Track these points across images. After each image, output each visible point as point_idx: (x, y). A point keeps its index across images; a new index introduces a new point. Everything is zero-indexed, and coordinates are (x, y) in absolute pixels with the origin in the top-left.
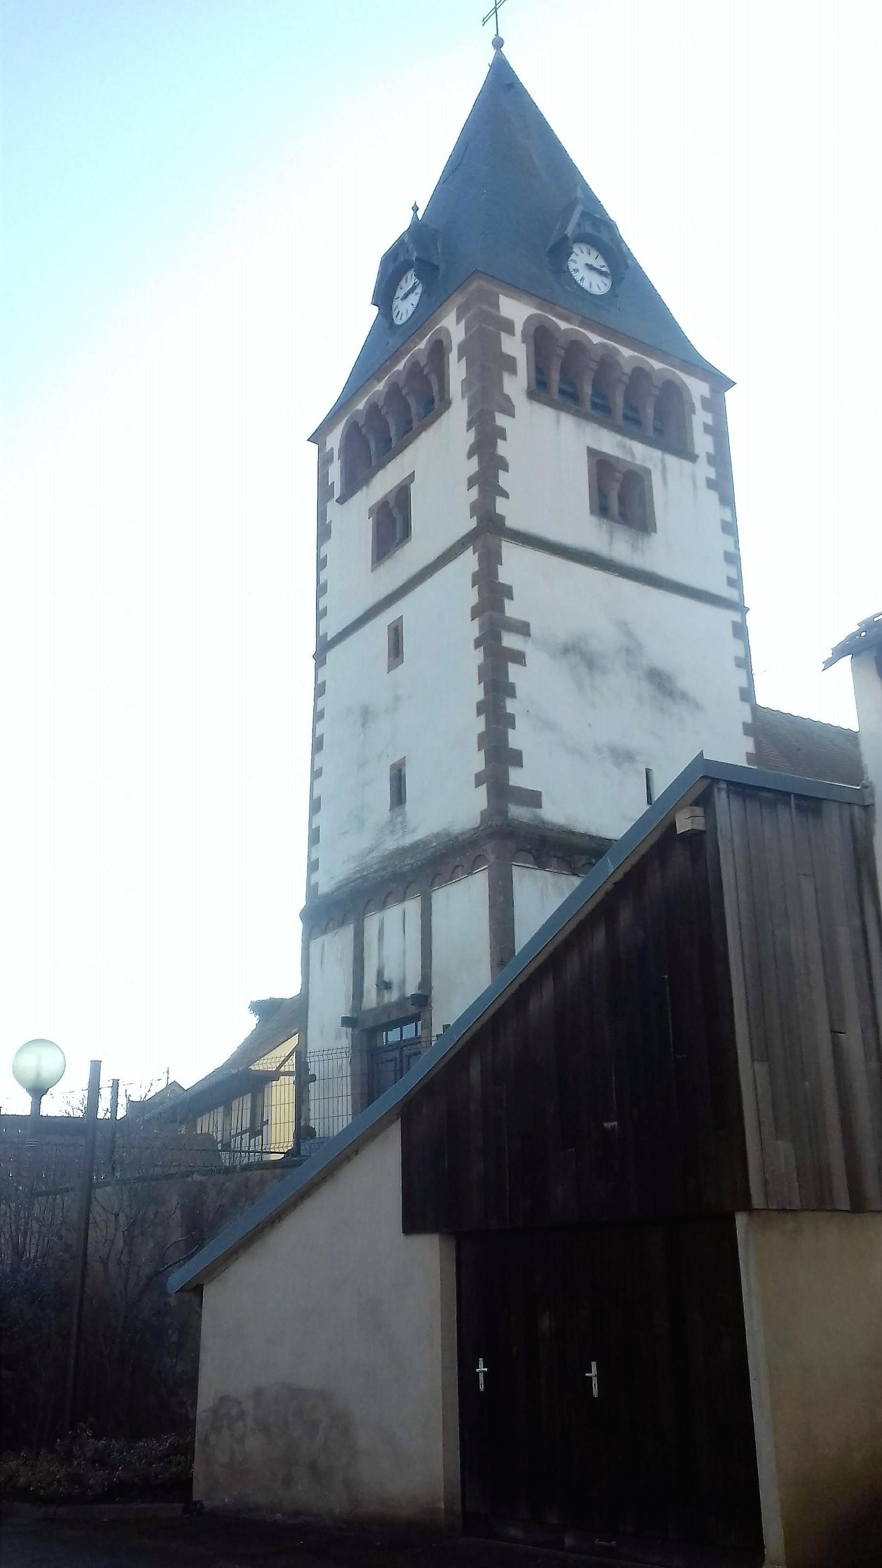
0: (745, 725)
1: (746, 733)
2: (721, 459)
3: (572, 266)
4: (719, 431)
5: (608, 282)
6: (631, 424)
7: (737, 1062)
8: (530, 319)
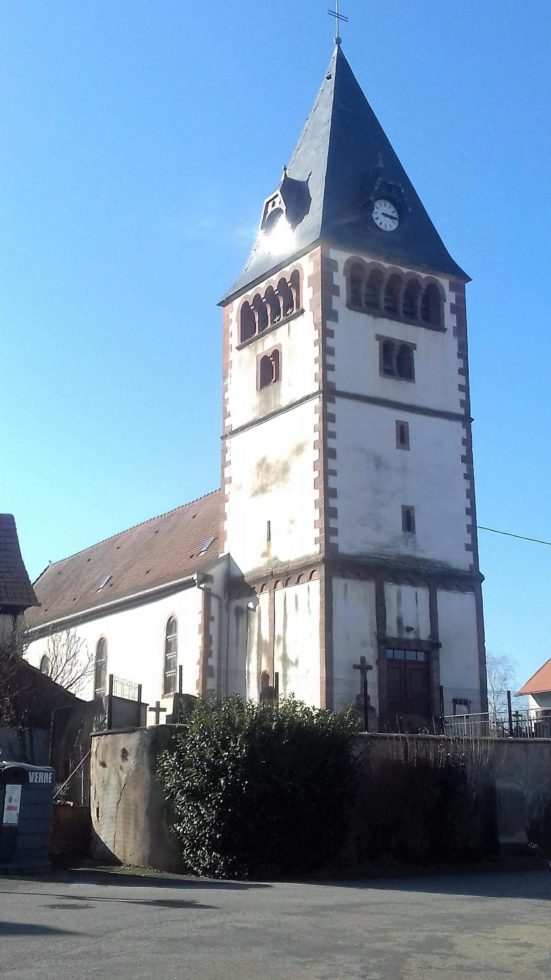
0: (462, 457)
1: (463, 444)
2: (461, 330)
3: (375, 216)
4: (460, 309)
5: (397, 222)
6: (409, 316)
7: (458, 266)
8: (348, 262)
